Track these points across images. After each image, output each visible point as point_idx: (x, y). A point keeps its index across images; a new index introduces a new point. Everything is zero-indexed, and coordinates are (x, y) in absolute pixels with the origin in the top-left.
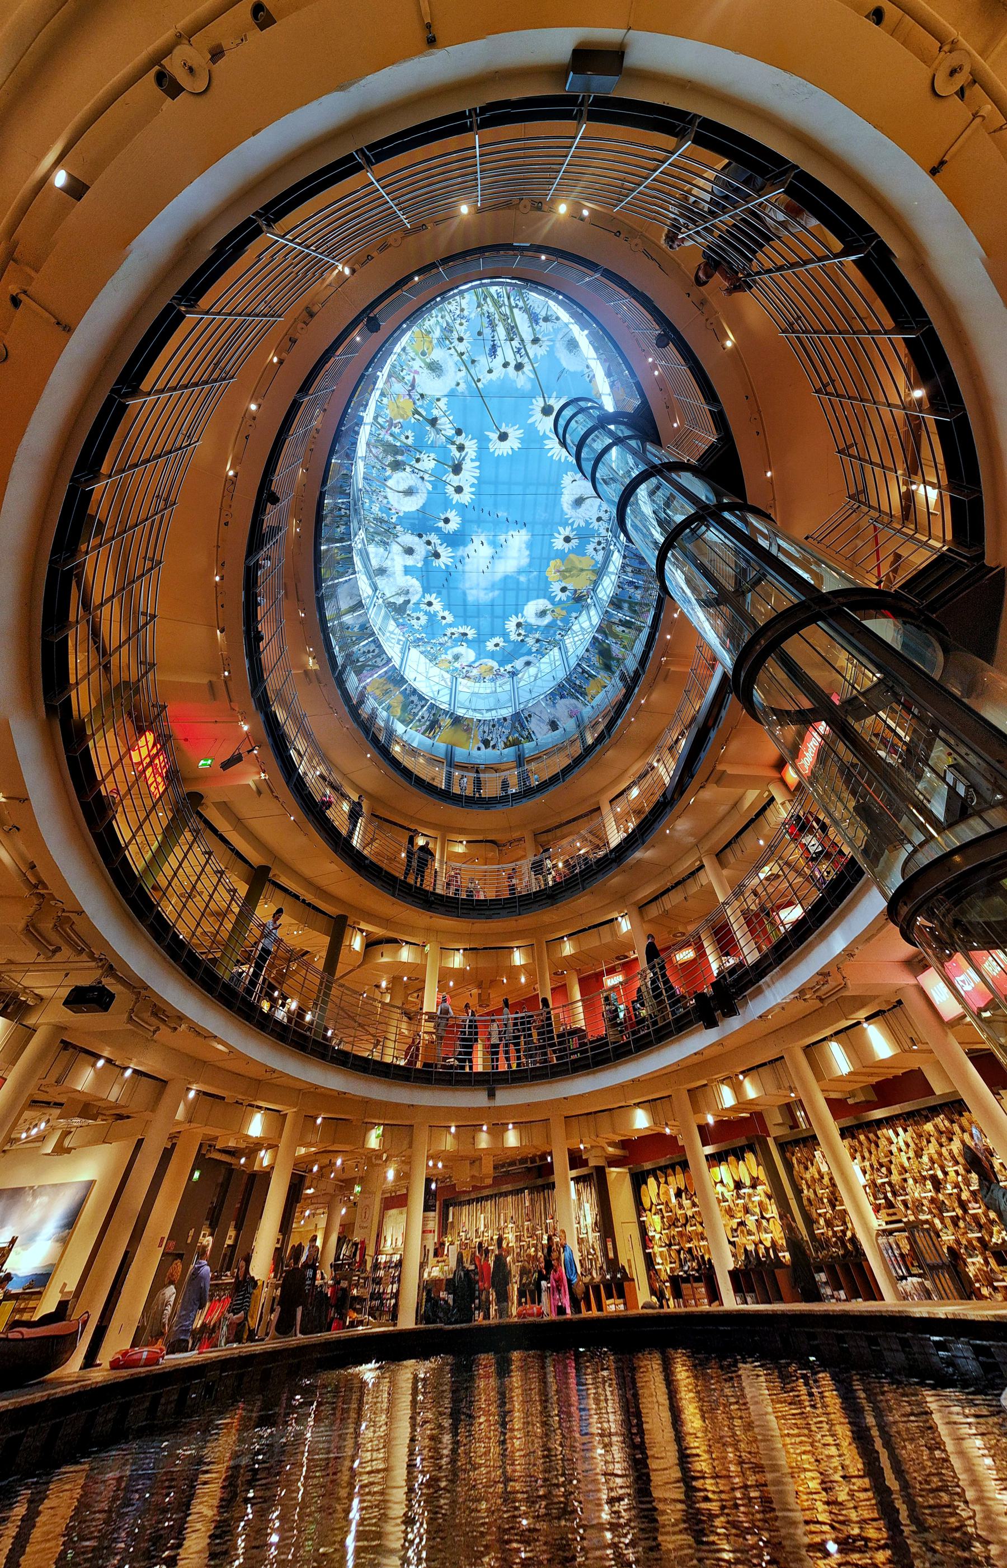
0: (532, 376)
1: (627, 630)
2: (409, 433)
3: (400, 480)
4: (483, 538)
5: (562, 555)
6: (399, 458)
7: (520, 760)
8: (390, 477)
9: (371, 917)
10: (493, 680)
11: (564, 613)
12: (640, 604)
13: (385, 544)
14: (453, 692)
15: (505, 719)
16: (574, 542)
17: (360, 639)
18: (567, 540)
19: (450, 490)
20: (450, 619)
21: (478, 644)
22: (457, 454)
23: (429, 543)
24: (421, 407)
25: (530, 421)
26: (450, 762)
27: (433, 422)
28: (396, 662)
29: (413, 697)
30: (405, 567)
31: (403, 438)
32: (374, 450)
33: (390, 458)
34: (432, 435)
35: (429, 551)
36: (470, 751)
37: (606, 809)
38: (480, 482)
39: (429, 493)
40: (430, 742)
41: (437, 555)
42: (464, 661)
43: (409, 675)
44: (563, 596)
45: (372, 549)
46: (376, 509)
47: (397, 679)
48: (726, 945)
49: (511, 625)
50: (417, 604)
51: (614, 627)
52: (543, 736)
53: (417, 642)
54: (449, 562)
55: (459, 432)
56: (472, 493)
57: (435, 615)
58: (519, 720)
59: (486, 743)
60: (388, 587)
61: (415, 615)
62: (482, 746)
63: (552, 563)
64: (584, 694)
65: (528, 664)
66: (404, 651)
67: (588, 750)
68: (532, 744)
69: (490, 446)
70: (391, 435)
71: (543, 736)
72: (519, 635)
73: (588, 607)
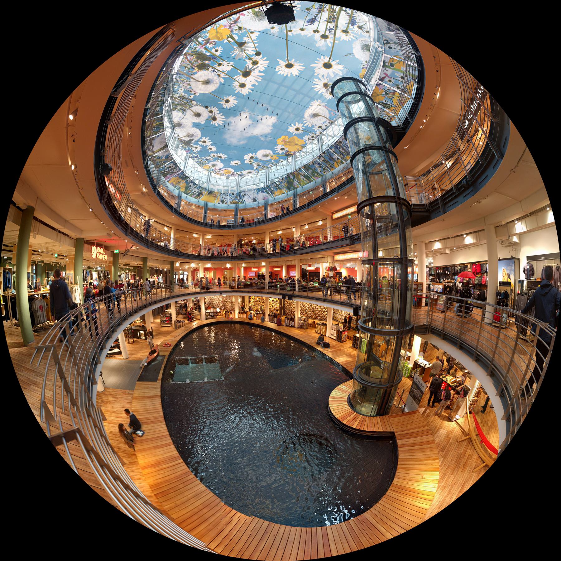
0: (330, 45)
3: (203, 75)
4: (247, 115)
5: (290, 134)
6: (206, 62)
7: (237, 210)
8: (196, 73)
12: (318, 174)
13: (183, 111)
17: (165, 162)
19: (236, 85)
20: (214, 149)
21: (226, 163)
23: (211, 112)
24: (236, 34)
25: (312, 65)
26: (206, 209)
27: (241, 45)
30: (194, 123)
31: (213, 51)
32: (189, 57)
33: (199, 62)
35: (210, 116)
36: (215, 203)
39: (221, 84)
41: (214, 119)
42: (217, 167)
43: (188, 173)
44: (281, 152)
49: (247, 157)
50: (197, 141)
52: (248, 201)
53: (194, 158)
54: (221, 123)
58: (240, 196)
59: (223, 202)
60: (181, 133)
61: (195, 146)
62: (221, 203)
64: (273, 193)
68: (243, 204)
69: (277, 67)
70: (205, 48)
71: (248, 201)
72: (250, 161)
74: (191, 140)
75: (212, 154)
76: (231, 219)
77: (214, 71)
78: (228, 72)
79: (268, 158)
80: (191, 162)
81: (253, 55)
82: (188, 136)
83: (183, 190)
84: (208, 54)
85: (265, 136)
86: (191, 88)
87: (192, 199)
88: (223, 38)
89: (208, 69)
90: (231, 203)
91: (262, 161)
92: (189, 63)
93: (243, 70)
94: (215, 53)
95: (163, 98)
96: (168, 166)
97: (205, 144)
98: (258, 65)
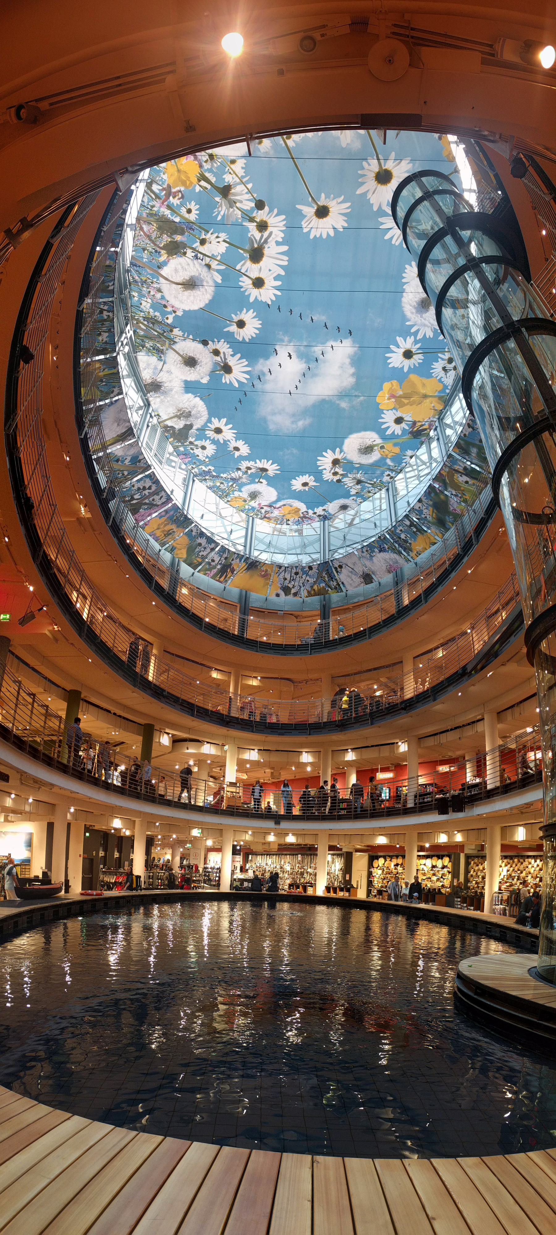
1: (471, 482)
2: (193, 206)
3: (178, 267)
4: (291, 349)
5: (398, 375)
6: (178, 238)
8: (165, 263)
9: (174, 726)
10: (298, 523)
11: (397, 450)
13: (159, 353)
14: (249, 535)
15: (310, 568)
16: (417, 359)
17: (134, 473)
18: (408, 354)
19: (246, 283)
20: (245, 450)
21: (280, 482)
22: (257, 235)
25: (359, 192)
26: (244, 606)
27: (225, 191)
28: (178, 498)
29: (199, 542)
30: (186, 382)
31: (183, 211)
33: (166, 239)
34: (223, 210)
35: (216, 364)
36: (266, 594)
37: (408, 666)
38: (289, 278)
39: (217, 285)
40: (222, 586)
41: (227, 369)
43: (194, 513)
44: (397, 429)
45: (143, 358)
46: (146, 305)
47: (180, 519)
48: (480, 770)
50: (202, 430)
51: (456, 476)
53: (203, 476)
54: (243, 378)
55: (260, 205)
56: (276, 288)
57: (226, 442)
58: (327, 570)
59: (287, 590)
60: (164, 407)
61: (199, 443)
62: (282, 593)
63: (387, 386)
64: (408, 549)
65: (344, 507)
66: (187, 484)
67: (402, 612)
69: (304, 224)
72: (335, 474)
73: (430, 440)
74: (189, 427)
75: (244, 465)
76: (306, 631)
77: (196, 257)
78: (223, 255)
79: (375, 456)
80: (200, 489)
81: (252, 210)
82: (179, 417)
83: (183, 554)
84: (177, 220)
85: (344, 395)
86: (163, 298)
87: (204, 580)
88: (191, 183)
89: (185, 254)
90: (310, 594)
91: (362, 467)
92: (147, 241)
93: (247, 247)
94: (187, 216)
95: (111, 314)
96: (141, 485)
97: (220, 437)
98: (270, 229)
